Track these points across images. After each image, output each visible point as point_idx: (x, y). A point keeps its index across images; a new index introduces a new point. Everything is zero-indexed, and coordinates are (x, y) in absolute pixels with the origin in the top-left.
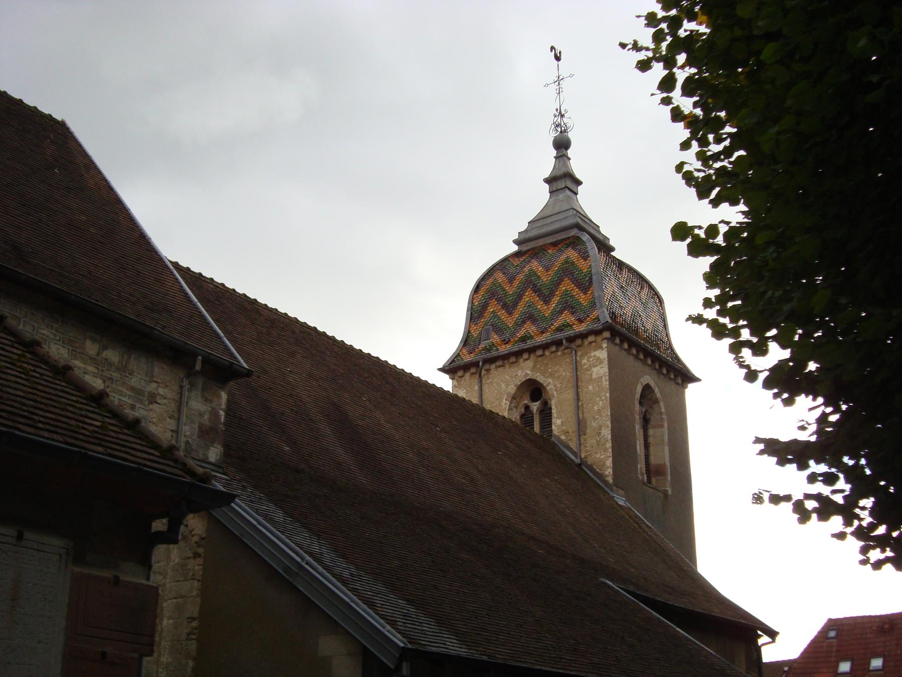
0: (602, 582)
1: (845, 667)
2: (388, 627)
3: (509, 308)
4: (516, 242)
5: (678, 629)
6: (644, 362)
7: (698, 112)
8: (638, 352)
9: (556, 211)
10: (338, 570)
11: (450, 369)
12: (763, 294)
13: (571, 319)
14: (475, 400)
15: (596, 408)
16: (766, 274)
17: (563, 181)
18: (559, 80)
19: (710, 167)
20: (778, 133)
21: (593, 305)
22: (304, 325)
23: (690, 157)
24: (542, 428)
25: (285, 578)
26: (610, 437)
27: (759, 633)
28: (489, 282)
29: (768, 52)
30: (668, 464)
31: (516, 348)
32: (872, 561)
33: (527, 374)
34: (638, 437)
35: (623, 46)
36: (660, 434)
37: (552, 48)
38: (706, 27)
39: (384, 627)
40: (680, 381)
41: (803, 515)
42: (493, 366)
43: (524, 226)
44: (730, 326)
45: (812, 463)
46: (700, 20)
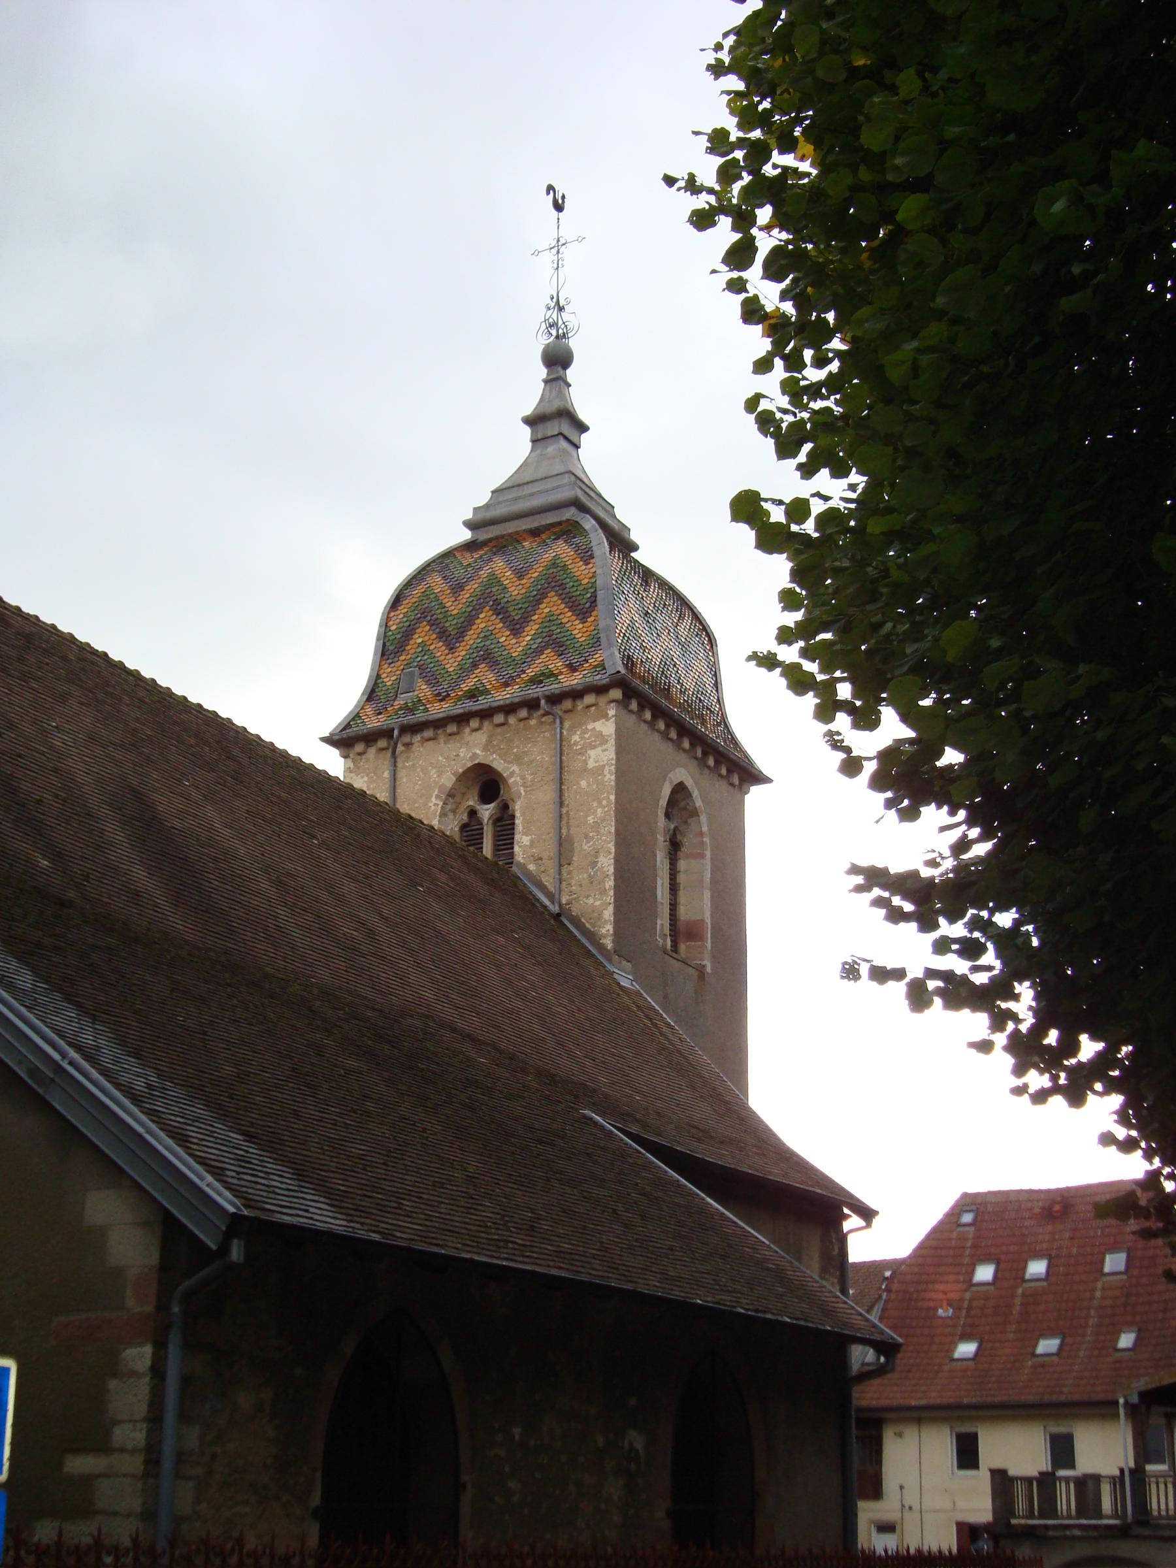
0: (585, 1117)
1: (984, 1273)
2: (210, 1179)
3: (450, 639)
4: (469, 525)
5: (709, 1200)
6: (678, 744)
7: (788, 308)
8: (668, 726)
9: (540, 474)
10: (124, 1078)
11: (345, 740)
12: (877, 627)
13: (557, 664)
14: (383, 796)
15: (591, 820)
16: (884, 590)
17: (556, 423)
18: (558, 246)
19: (805, 408)
20: (919, 351)
21: (596, 643)
22: (86, 648)
23: (771, 384)
24: (497, 849)
25: (32, 1088)
26: (612, 870)
27: (846, 1211)
28: (417, 592)
29: (909, 208)
30: (709, 921)
31: (458, 710)
32: (1031, 1091)
33: (475, 755)
34: (660, 873)
35: (670, 181)
36: (697, 870)
37: (550, 188)
38: (812, 165)
39: (202, 1179)
40: (736, 780)
41: (918, 997)
42: (417, 738)
43: (484, 498)
44: (820, 677)
45: (942, 920)
46: (800, 152)
